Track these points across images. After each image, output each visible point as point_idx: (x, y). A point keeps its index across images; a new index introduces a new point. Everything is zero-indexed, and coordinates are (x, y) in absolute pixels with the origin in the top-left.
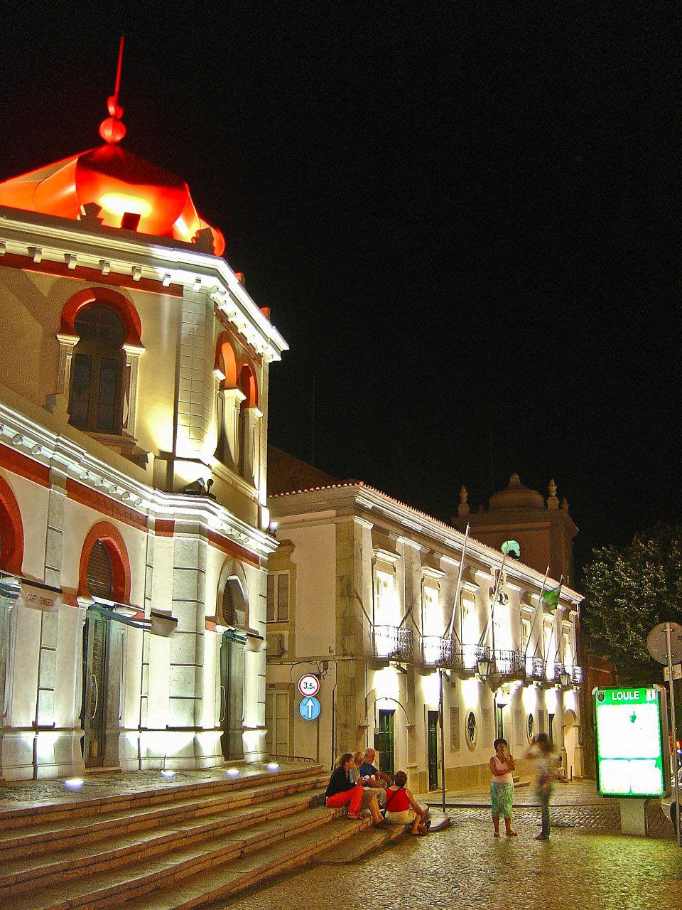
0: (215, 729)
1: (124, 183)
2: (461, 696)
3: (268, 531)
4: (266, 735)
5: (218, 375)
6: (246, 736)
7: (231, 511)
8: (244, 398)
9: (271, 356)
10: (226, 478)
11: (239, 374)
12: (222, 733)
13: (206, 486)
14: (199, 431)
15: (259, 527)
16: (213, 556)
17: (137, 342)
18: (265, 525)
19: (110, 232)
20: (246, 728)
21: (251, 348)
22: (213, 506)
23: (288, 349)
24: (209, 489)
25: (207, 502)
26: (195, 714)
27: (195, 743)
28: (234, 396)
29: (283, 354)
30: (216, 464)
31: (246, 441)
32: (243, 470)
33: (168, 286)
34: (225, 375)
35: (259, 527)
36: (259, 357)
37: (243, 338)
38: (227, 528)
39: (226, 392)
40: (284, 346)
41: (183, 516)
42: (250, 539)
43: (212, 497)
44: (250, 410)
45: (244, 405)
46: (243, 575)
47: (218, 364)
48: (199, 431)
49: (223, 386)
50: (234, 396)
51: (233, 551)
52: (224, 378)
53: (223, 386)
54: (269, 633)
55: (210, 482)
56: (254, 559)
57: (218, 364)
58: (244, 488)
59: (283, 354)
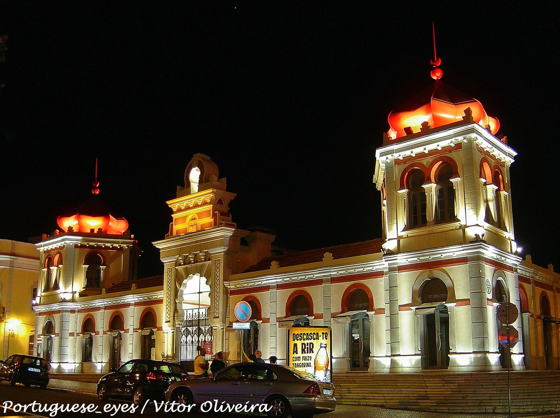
1: (88, 216)
3: (516, 253)
7: (496, 247)
9: (509, 161)
11: (493, 176)
13: (481, 237)
16: (488, 270)
18: (514, 251)
19: (418, 135)
22: (445, 250)
23: (517, 154)
24: (482, 238)
27: (60, 365)
28: (491, 188)
29: (515, 158)
30: (487, 225)
32: (500, 225)
33: (415, 156)
35: (511, 253)
38: (495, 256)
40: (515, 154)
41: (101, 305)
42: (507, 259)
43: (485, 242)
44: (501, 192)
45: (497, 192)
46: (504, 277)
49: (485, 184)
50: (491, 188)
51: (499, 266)
52: (485, 181)
54: (30, 343)
55: (483, 235)
58: (501, 233)
59: (515, 158)
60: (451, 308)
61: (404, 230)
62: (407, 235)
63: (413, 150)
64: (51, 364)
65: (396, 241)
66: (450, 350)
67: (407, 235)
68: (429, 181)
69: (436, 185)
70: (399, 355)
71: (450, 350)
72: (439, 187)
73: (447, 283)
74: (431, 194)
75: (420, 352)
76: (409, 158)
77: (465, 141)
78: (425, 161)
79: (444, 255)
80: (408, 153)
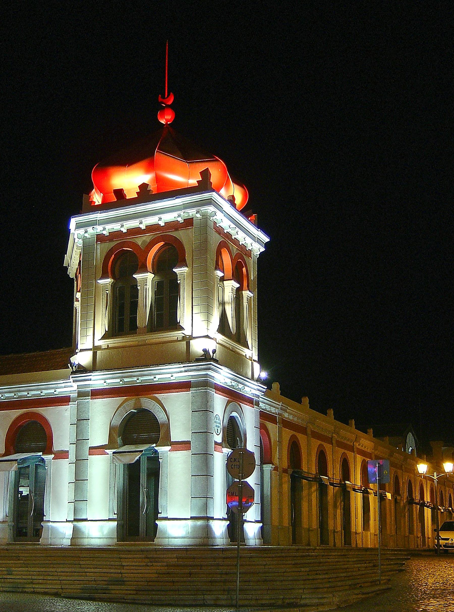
0: (224, 519)
2: (179, 181)
4: (262, 528)
5: (220, 274)
6: (247, 526)
7: (232, 370)
8: (238, 285)
10: (224, 343)
12: (228, 522)
13: (211, 354)
14: (208, 312)
15: (253, 378)
17: (183, 263)
20: (246, 521)
21: (243, 248)
23: (269, 240)
24: (213, 355)
25: (210, 364)
26: (206, 507)
30: (220, 338)
31: (241, 320)
34: (224, 273)
35: (253, 378)
36: (249, 253)
37: (236, 242)
38: (229, 382)
39: (225, 282)
42: (246, 387)
43: (216, 361)
45: (238, 292)
46: (241, 413)
47: (218, 266)
48: (208, 312)
49: (222, 279)
52: (222, 275)
53: (222, 279)
55: (214, 351)
56: (250, 401)
57: (218, 266)
60: (163, 453)
61: (104, 338)
62: (108, 346)
63: (162, 216)
64: (157, 522)
65: (91, 353)
66: (159, 514)
67: (108, 346)
68: (144, 269)
69: (153, 275)
70: (86, 520)
71: (159, 514)
72: (157, 279)
73: (161, 417)
74: (145, 288)
75: (115, 516)
76: (115, 235)
77: (198, 215)
78: (140, 241)
79: (158, 377)
80: (116, 227)
